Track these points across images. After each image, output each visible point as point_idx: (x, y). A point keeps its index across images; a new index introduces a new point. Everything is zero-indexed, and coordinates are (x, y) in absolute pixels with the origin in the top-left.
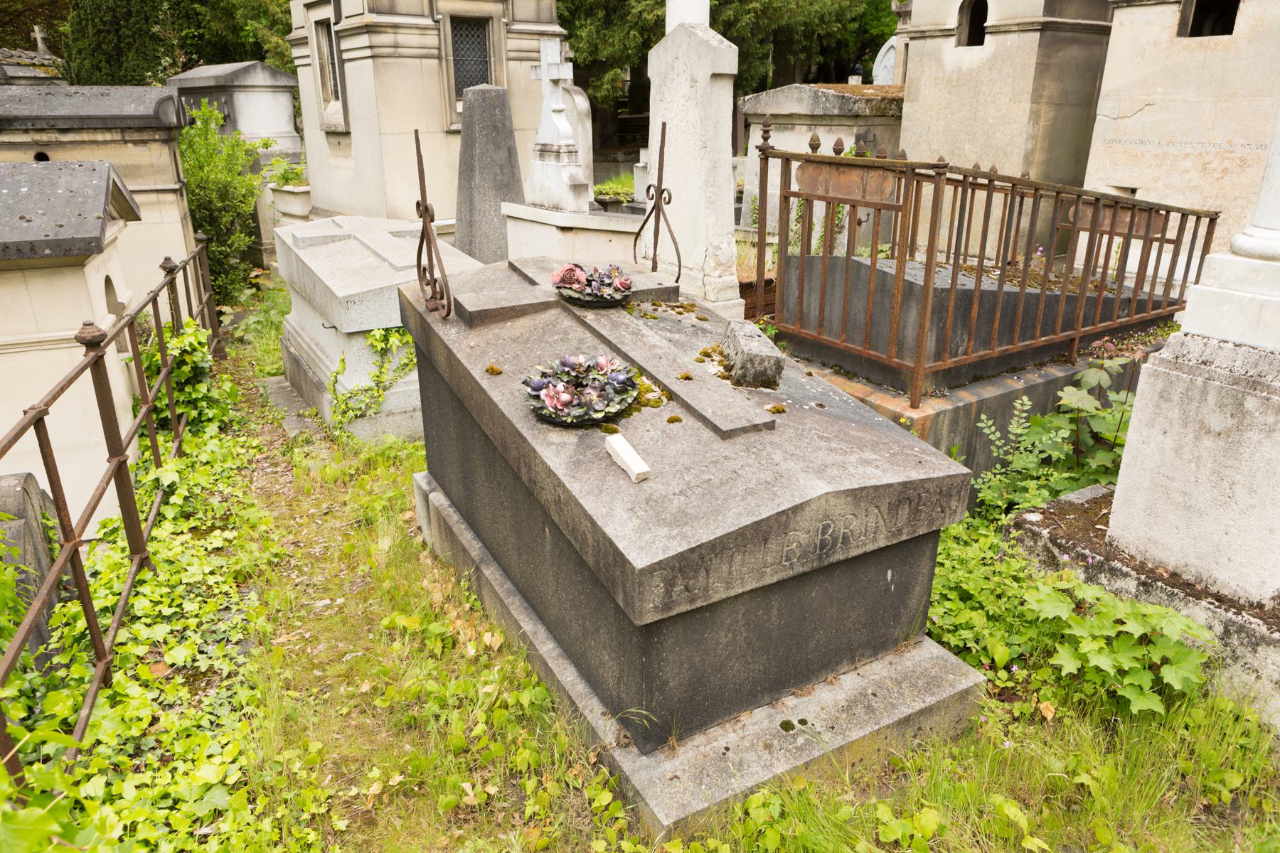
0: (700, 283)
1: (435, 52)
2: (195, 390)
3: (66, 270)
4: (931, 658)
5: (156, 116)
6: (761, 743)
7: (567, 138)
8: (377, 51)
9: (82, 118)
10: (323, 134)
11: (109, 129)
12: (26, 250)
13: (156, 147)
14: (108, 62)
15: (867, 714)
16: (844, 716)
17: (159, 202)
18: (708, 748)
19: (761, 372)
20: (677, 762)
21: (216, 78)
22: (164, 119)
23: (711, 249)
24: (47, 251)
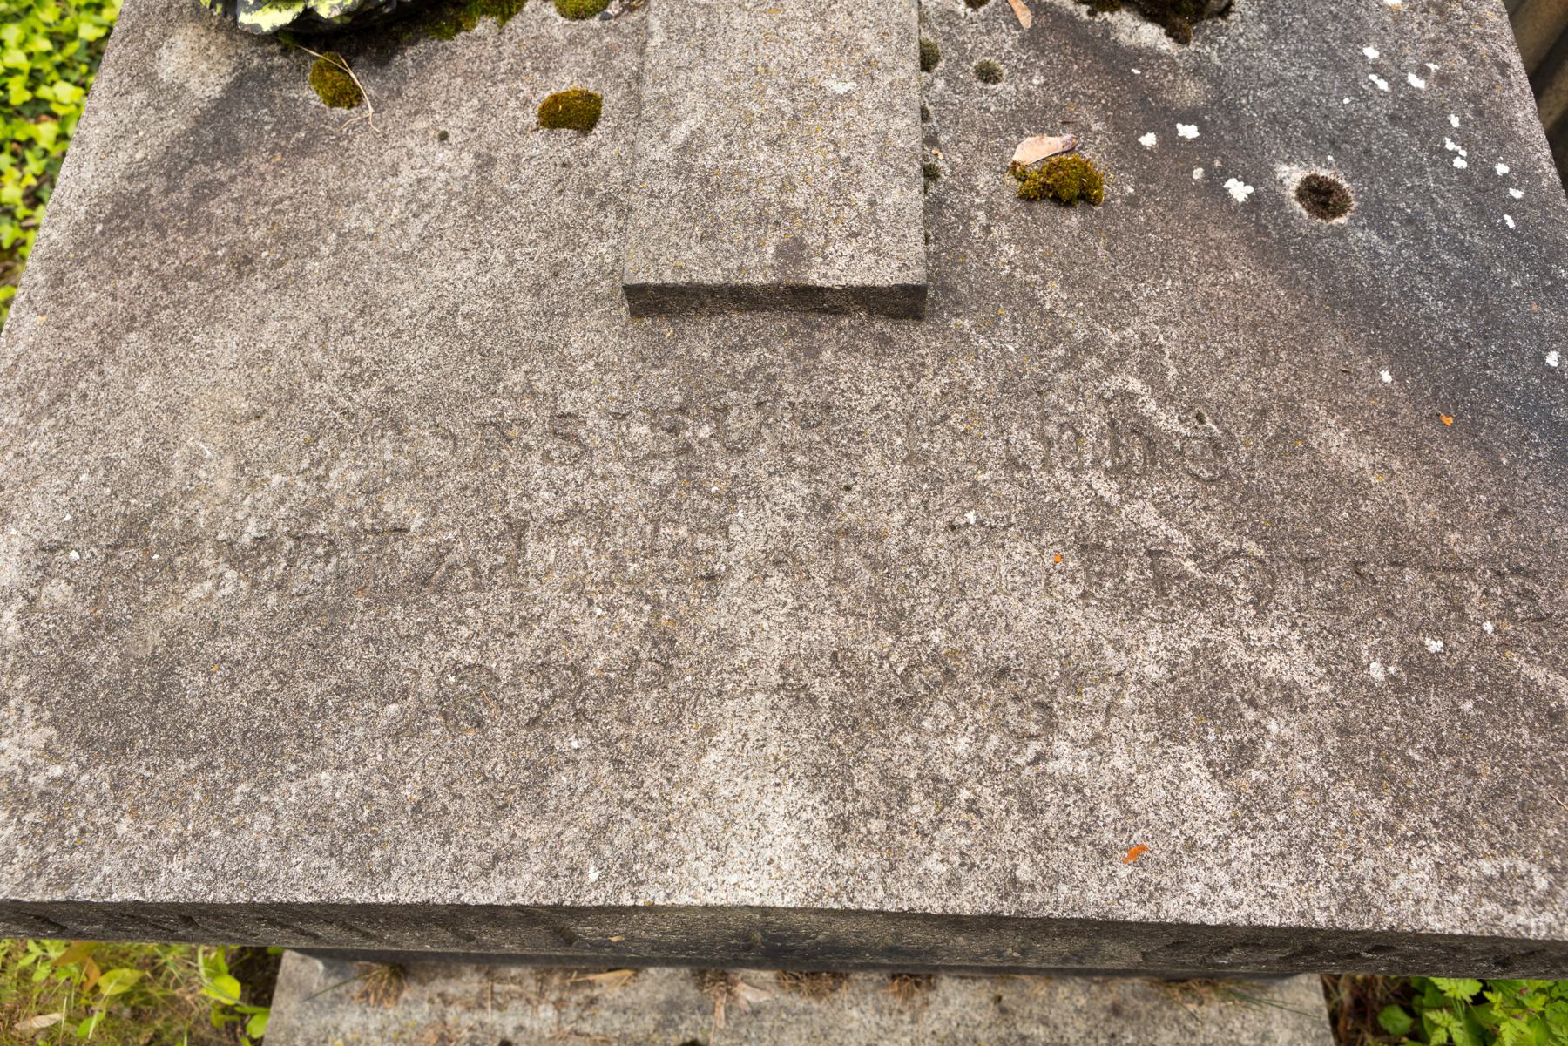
18: (469, 1019)
20: (374, 1022)
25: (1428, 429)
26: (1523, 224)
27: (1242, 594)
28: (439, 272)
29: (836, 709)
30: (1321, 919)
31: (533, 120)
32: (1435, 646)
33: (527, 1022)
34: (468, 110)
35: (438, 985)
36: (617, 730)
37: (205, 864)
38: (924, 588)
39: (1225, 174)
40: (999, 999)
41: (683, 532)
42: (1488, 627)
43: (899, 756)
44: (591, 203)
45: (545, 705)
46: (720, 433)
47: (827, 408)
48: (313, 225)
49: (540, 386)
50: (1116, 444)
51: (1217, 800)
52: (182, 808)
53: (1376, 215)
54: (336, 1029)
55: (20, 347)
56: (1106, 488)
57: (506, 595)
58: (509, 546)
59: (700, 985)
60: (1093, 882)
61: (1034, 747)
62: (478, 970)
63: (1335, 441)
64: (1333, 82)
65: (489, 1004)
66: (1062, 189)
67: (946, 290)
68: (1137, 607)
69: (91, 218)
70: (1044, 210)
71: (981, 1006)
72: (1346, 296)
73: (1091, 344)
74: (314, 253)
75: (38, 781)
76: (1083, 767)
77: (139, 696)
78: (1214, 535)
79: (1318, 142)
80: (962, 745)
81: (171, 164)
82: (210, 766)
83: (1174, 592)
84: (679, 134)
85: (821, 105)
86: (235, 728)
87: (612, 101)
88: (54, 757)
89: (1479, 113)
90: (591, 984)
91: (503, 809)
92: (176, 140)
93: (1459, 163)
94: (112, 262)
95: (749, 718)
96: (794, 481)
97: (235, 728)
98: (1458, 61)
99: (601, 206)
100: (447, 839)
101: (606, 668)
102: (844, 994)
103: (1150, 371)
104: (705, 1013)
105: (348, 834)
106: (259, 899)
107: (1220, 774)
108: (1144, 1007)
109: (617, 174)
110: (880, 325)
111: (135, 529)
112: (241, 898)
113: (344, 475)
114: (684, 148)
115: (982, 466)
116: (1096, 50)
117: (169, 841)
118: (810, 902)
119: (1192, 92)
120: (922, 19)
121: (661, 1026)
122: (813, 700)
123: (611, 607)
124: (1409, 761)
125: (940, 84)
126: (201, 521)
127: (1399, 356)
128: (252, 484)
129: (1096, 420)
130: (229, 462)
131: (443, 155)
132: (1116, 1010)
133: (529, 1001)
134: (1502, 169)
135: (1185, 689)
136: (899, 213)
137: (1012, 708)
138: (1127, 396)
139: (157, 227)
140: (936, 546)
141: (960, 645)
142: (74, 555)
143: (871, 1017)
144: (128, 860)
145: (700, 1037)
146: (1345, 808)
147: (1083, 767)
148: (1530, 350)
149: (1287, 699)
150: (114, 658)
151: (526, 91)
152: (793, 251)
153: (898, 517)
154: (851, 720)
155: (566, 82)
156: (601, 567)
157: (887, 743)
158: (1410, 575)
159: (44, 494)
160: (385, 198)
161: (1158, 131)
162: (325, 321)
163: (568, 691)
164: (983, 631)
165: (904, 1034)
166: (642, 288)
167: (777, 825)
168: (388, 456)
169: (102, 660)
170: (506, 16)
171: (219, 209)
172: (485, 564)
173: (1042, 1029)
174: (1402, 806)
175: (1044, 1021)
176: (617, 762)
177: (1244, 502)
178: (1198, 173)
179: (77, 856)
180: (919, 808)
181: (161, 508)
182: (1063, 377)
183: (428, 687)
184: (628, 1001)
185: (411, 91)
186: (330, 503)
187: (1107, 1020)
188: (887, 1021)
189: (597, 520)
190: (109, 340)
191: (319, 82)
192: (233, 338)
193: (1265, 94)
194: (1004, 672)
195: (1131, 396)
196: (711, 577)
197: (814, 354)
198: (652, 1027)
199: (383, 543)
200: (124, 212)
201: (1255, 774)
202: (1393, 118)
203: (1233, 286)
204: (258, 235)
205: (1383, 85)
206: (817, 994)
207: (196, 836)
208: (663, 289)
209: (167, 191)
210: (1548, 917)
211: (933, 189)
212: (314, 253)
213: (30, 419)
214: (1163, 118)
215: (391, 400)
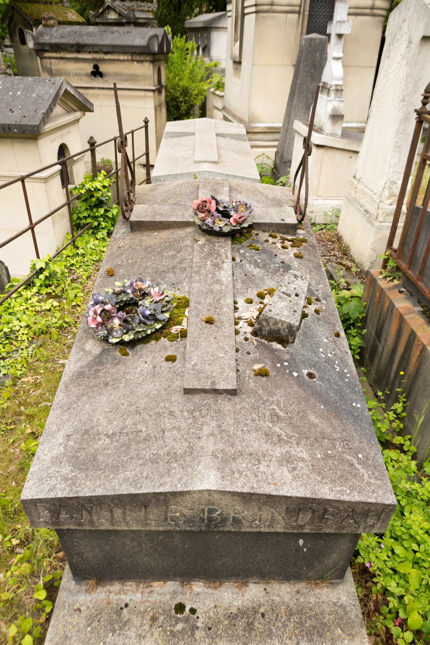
0: (376, 206)
1: (297, 8)
2: (97, 211)
3: (29, 140)
4: (335, 604)
5: (148, 46)
6: (151, 614)
7: (338, 79)
8: (260, 8)
9: (114, 46)
10: (231, 62)
11: (125, 53)
12: (7, 128)
13: (147, 64)
14: (174, 10)
15: (244, 630)
16: (226, 622)
17: (145, 97)
18: (116, 597)
19: (274, 330)
20: (89, 599)
21: (204, 22)
22: (151, 48)
23: (388, 183)
24: (16, 131)
25: (330, 416)
26: (350, 381)
27: (294, 443)
28: (146, 386)
29: (222, 459)
30: (308, 496)
31: (164, 360)
32: (330, 452)
33: (133, 598)
34: (151, 357)
35: (108, 587)
36: (183, 463)
37: (105, 488)
38: (237, 440)
39: (293, 371)
40: (265, 589)
41: (194, 430)
42: (340, 449)
43: (233, 467)
44: (175, 375)
45: (170, 459)
46: (201, 414)
47: (220, 410)
48: (120, 378)
49: (167, 406)
50: (272, 417)
51: (290, 476)
52: (100, 479)
53: (321, 379)
54: (77, 601)
55: (59, 399)
56: (270, 425)
57: (162, 442)
58: (162, 433)
59: (182, 586)
60: (267, 488)
61: (256, 466)
62: (119, 583)
63: (312, 418)
64: (314, 355)
65: (122, 593)
66: (262, 373)
67: (241, 391)
68: (275, 444)
69: (73, 375)
70: (259, 377)
71: (261, 591)
72: (315, 393)
73: (267, 400)
74: (121, 383)
75: (70, 476)
76: (265, 470)
77: (90, 461)
78: (289, 433)
79: (311, 366)
80: (244, 465)
81: (90, 366)
82: (105, 472)
83: (282, 442)
84: (193, 363)
85: (218, 358)
86: (110, 465)
87: (179, 357)
88: (72, 471)
89: (342, 361)
90: (151, 586)
91: (162, 476)
92: (90, 361)
93: (338, 370)
94: (78, 384)
95: (206, 460)
96: (214, 422)
97: (110, 465)
98: (338, 352)
99: (177, 375)
100: (152, 482)
101: (181, 453)
102: (223, 589)
103: (278, 405)
104: (184, 595)
105: (133, 482)
106: (116, 494)
107: (290, 472)
108: (305, 591)
109: (180, 370)
110: (229, 396)
111: (87, 432)
112: (112, 494)
113: (129, 422)
114: (194, 365)
115: (247, 420)
116: (269, 349)
117: (98, 485)
118: (218, 489)
119: (287, 357)
120: (236, 343)
121: (171, 599)
122: (218, 457)
123: (181, 443)
124: (325, 471)
125: (240, 355)
126: (101, 430)
127: (325, 403)
128: (111, 424)
129: (268, 413)
130: (106, 420)
131: (146, 366)
132: (298, 592)
133: (134, 592)
134: (346, 371)
135: (284, 458)
136: (232, 377)
137: (253, 460)
138: (274, 409)
139: (87, 377)
140: (239, 433)
141: (244, 449)
142: (74, 437)
143: (230, 595)
144: (89, 489)
145: (182, 602)
146: (313, 478)
147: (265, 470)
148: (350, 403)
149: (302, 460)
150: (84, 454)
151: (162, 354)
152: (213, 383)
153: (232, 428)
154: (224, 462)
155: (170, 353)
156: (179, 436)
157: (231, 464)
158: (326, 440)
159: (67, 426)
160: (135, 373)
161: (280, 364)
162: (124, 395)
163: (173, 456)
164: (248, 447)
165: (240, 600)
166: (187, 389)
167: (212, 477)
168: (138, 418)
169: (82, 455)
170: (157, 341)
171: (101, 374)
172: (157, 437)
173: (278, 598)
174: (323, 478)
175: (278, 595)
176: (183, 468)
177: (295, 427)
178: (288, 371)
179: (79, 489)
180: (236, 475)
181: (92, 428)
182: (262, 406)
183: (147, 457)
184: (162, 591)
185: (139, 354)
186: (127, 427)
187: (296, 595)
188: (235, 596)
189: (178, 429)
190: (79, 398)
191: (120, 351)
192: (105, 398)
193: (301, 357)
194: (251, 454)
195: (275, 409)
196: (199, 438)
197: (217, 401)
198: (169, 599)
199: (137, 434)
200: (80, 375)
201: (296, 472)
202: (325, 362)
203: (294, 391)
204: (109, 379)
205: (323, 356)
206: (215, 588)
207: (103, 484)
208: (190, 389)
209: (89, 371)
210: (349, 497)
211: (238, 373)
212: (121, 383)
213: (62, 412)
214: (281, 361)
215: (138, 409)
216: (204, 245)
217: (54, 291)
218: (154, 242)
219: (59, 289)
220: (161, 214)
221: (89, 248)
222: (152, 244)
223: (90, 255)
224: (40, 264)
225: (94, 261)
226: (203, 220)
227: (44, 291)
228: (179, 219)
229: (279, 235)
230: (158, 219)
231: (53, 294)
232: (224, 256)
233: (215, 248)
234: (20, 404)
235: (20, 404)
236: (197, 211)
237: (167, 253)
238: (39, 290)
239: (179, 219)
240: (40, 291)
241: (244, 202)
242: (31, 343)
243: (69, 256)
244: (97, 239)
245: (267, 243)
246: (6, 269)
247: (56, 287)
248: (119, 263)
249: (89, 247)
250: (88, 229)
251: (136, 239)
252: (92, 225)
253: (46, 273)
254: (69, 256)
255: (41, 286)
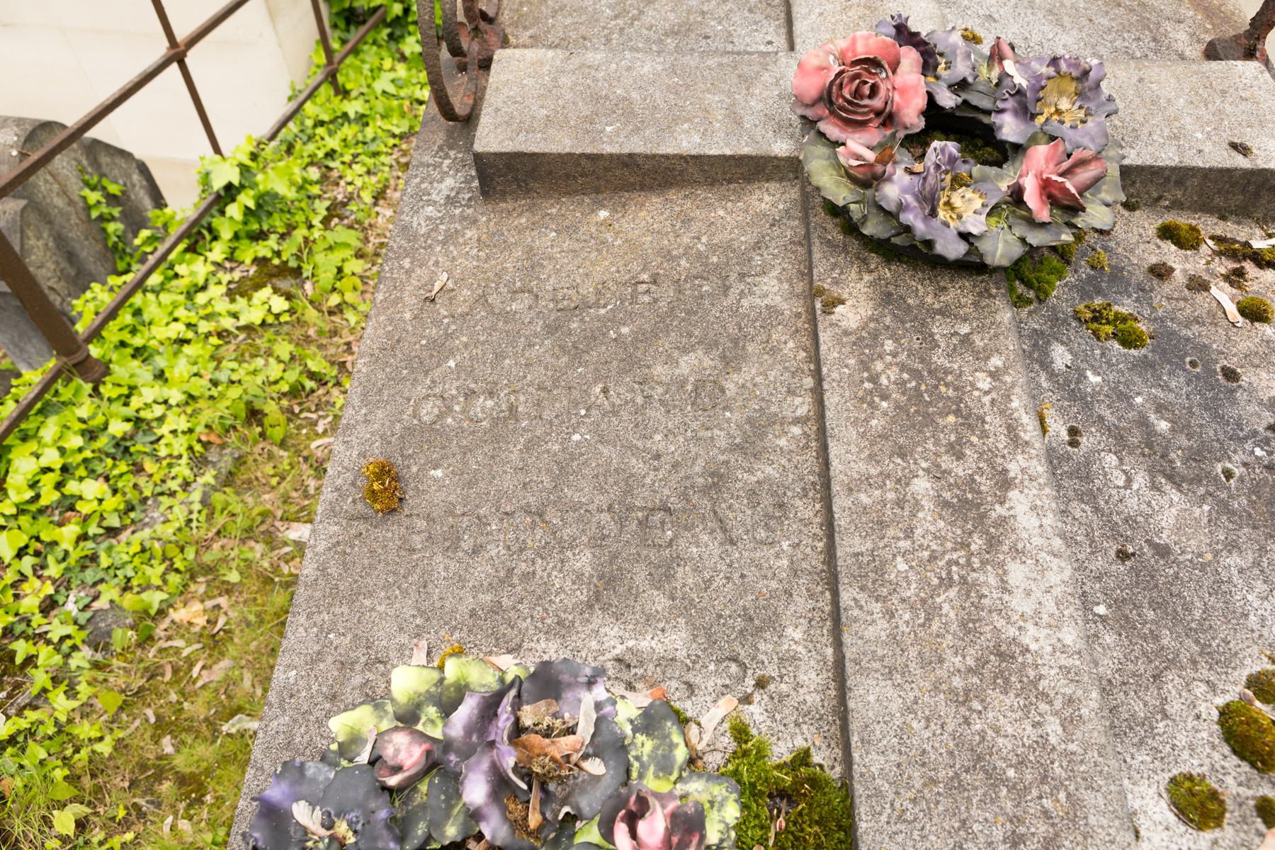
216: (875, 336)
217: (278, 254)
218: (598, 273)
219: (289, 249)
220: (624, 110)
221: (379, 92)
222: (588, 289)
223: (383, 117)
224: (226, 174)
225: (394, 136)
226: (868, 180)
227: (248, 252)
228: (718, 147)
229: (1209, 226)
230: (614, 140)
231: (276, 261)
232: (994, 422)
233: (939, 359)
234: (162, 726)
235: (162, 726)
236: (822, 110)
237: (670, 361)
238: (233, 250)
239: (720, 144)
240: (237, 254)
241: (1075, 63)
242: (200, 462)
243: (322, 123)
244: (403, 58)
245: (1167, 288)
246: (143, 169)
247: (283, 236)
248: (429, 411)
249: (378, 90)
250: (375, 27)
251: (508, 247)
252: (385, 13)
253: (247, 199)
254: (322, 123)
255: (236, 237)
